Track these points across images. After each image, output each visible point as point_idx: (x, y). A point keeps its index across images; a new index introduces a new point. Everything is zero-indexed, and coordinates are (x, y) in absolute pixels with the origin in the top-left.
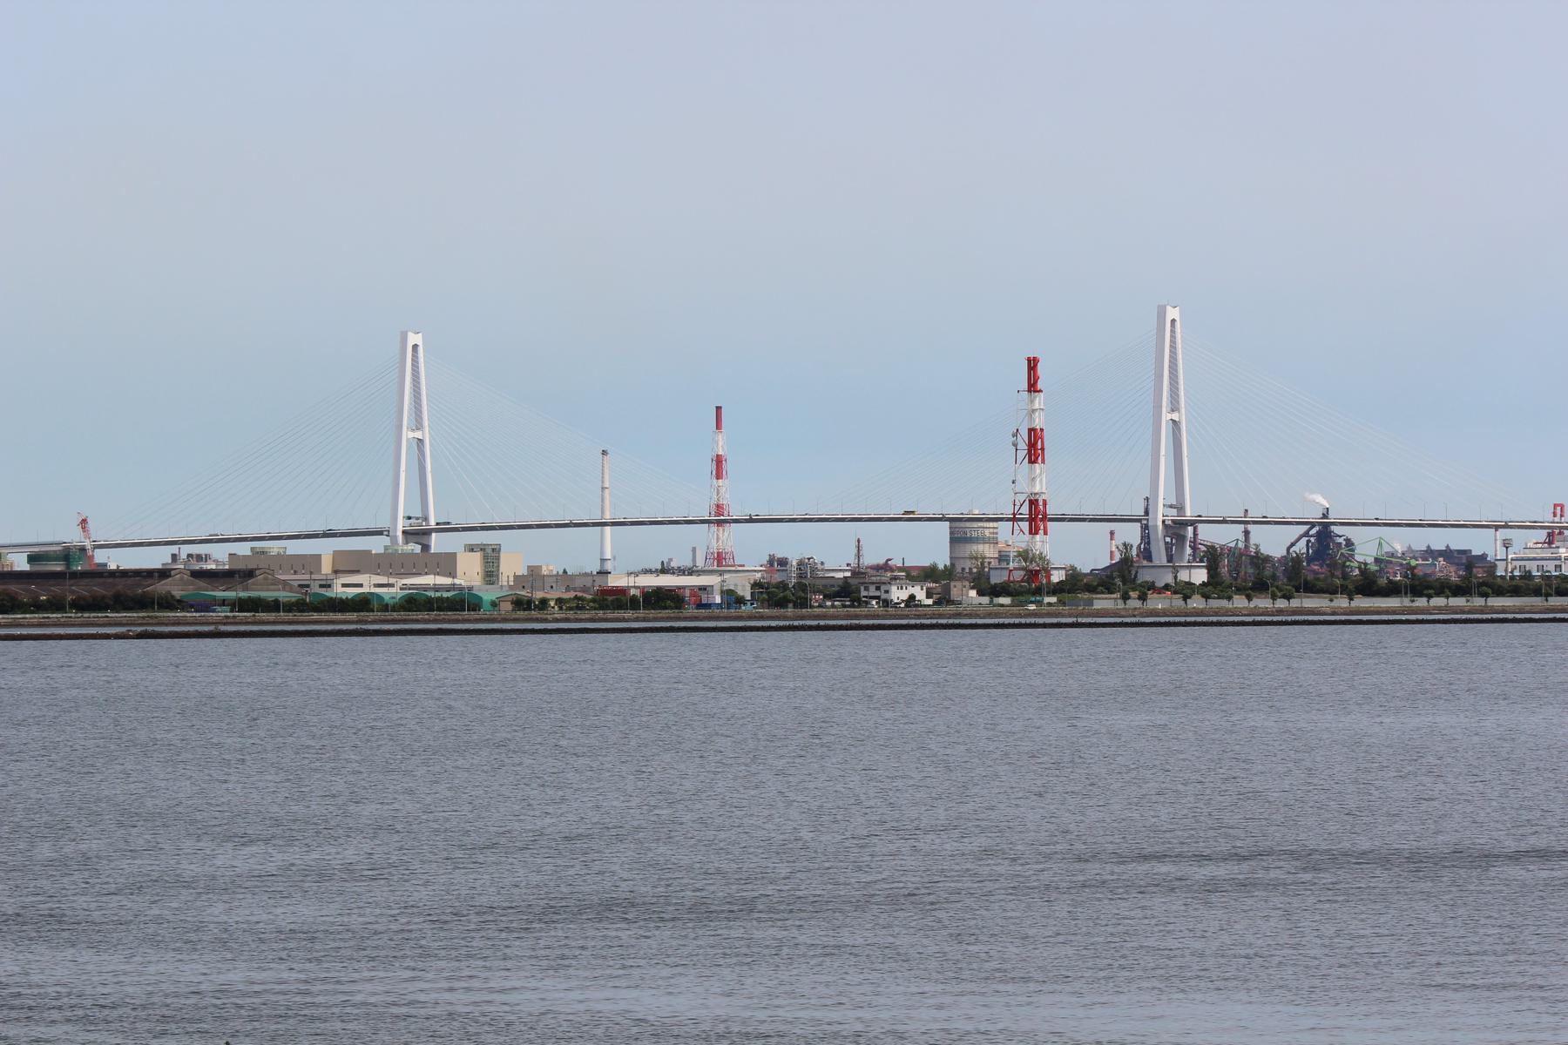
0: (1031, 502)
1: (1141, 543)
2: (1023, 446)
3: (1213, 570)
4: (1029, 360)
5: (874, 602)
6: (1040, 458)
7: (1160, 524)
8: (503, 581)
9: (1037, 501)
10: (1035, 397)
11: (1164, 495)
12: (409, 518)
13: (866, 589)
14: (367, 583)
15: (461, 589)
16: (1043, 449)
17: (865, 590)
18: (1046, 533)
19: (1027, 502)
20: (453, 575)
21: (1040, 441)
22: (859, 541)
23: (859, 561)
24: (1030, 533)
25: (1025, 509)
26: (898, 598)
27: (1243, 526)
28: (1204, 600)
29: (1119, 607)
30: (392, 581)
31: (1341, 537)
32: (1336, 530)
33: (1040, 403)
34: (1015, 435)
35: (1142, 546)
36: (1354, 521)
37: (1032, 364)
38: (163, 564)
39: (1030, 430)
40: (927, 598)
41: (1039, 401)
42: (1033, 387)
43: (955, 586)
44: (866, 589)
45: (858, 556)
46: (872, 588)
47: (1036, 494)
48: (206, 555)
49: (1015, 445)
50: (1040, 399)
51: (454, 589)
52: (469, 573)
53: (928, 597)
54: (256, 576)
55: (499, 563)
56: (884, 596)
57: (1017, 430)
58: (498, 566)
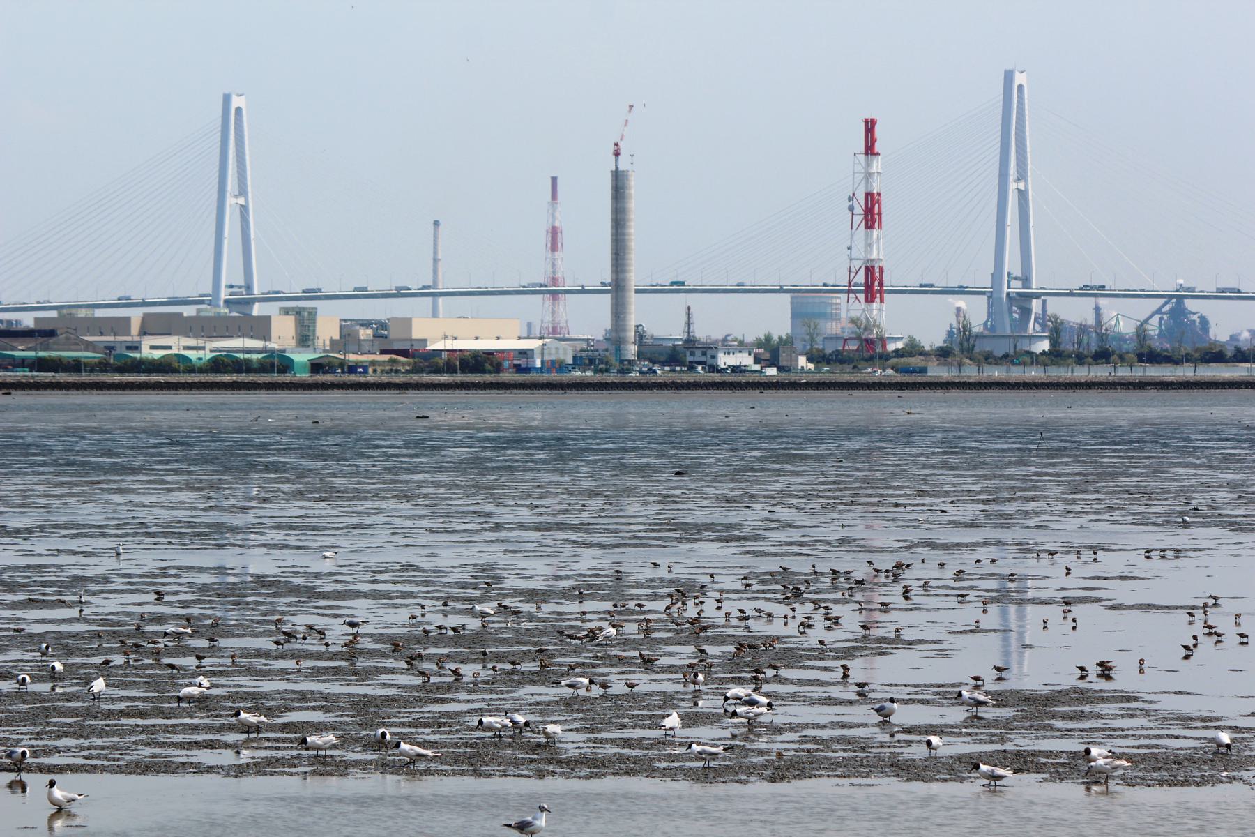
0: (867, 269)
1: (987, 321)
2: (859, 210)
3: (1055, 342)
4: (866, 121)
5: (700, 368)
6: (876, 224)
7: (1004, 296)
8: (319, 344)
9: (873, 267)
10: (872, 160)
11: (1012, 264)
12: (232, 287)
13: (692, 354)
14: (177, 344)
15: (272, 352)
16: (880, 214)
17: (691, 355)
18: (882, 301)
19: (863, 269)
20: (266, 337)
21: (877, 206)
22: (689, 308)
23: (689, 328)
24: (866, 300)
25: (860, 278)
26: (725, 364)
27: (1093, 299)
28: (1043, 368)
29: (954, 374)
30: (201, 343)
31: (1194, 314)
32: (1190, 305)
33: (877, 167)
34: (851, 199)
35: (989, 323)
36: (1206, 294)
37: (870, 126)
38: (9, 394)
39: (867, 195)
40: (755, 363)
41: (877, 165)
42: (870, 150)
43: (784, 352)
44: (692, 354)
45: (689, 324)
46: (698, 353)
47: (872, 260)
48: (16, 321)
49: (851, 209)
50: (877, 162)
51: (266, 352)
52: (283, 335)
53: (756, 362)
54: (57, 335)
55: (315, 326)
56: (710, 361)
57: (854, 194)
58: (314, 331)
